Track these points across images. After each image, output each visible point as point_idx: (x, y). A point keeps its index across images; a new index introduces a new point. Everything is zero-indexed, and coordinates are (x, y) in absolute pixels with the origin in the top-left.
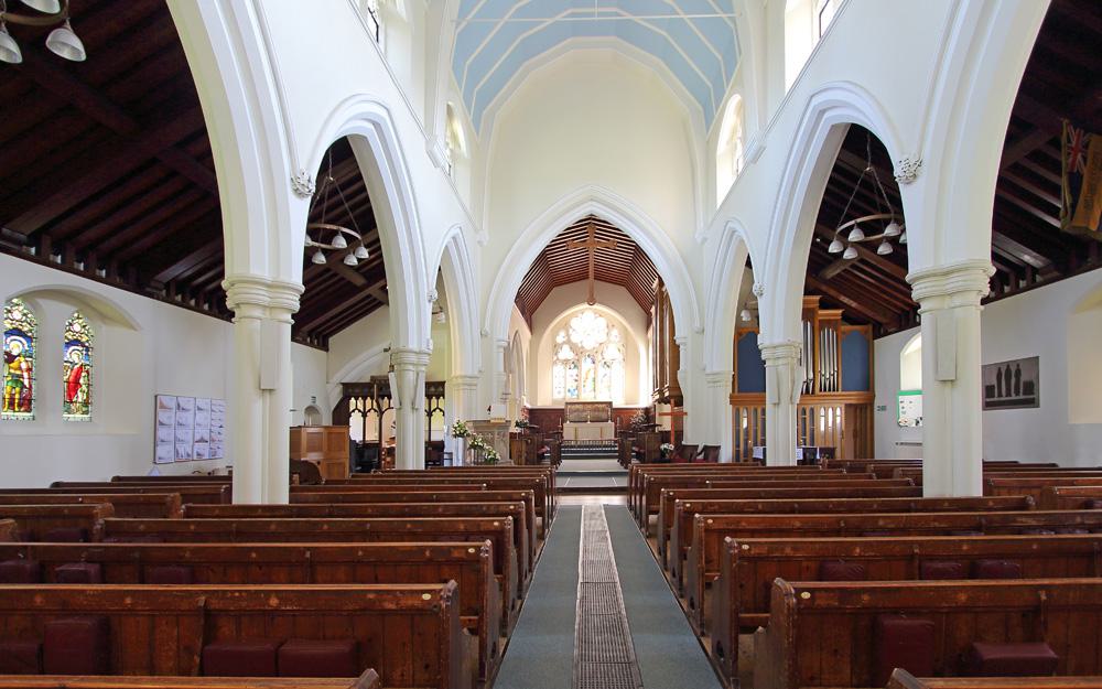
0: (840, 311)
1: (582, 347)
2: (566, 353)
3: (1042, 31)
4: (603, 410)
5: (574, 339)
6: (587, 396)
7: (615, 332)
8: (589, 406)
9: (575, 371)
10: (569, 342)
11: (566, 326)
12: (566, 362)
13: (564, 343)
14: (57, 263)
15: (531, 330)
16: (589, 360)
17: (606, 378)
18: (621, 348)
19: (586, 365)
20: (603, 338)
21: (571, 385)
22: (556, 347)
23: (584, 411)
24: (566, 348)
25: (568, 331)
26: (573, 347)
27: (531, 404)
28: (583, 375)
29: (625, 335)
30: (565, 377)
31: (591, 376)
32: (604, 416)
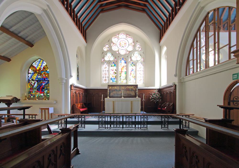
0: (2, 126)
1: (119, 53)
2: (109, 57)
3: (73, 121)
4: (132, 90)
5: (114, 48)
6: (122, 81)
7: (138, 46)
8: (123, 88)
9: (115, 68)
10: (110, 50)
11: (109, 41)
12: (109, 62)
13: (108, 51)
14: (228, 109)
15: (85, 39)
16: (123, 61)
17: (133, 72)
18: (142, 54)
19: (122, 64)
20: (130, 49)
21: (112, 75)
22: (104, 54)
23: (120, 90)
24: (109, 55)
25: (110, 45)
26: (114, 54)
27: (221, 60)
28: (120, 70)
29: (145, 47)
30: (108, 71)
31: (124, 70)
32: (133, 94)
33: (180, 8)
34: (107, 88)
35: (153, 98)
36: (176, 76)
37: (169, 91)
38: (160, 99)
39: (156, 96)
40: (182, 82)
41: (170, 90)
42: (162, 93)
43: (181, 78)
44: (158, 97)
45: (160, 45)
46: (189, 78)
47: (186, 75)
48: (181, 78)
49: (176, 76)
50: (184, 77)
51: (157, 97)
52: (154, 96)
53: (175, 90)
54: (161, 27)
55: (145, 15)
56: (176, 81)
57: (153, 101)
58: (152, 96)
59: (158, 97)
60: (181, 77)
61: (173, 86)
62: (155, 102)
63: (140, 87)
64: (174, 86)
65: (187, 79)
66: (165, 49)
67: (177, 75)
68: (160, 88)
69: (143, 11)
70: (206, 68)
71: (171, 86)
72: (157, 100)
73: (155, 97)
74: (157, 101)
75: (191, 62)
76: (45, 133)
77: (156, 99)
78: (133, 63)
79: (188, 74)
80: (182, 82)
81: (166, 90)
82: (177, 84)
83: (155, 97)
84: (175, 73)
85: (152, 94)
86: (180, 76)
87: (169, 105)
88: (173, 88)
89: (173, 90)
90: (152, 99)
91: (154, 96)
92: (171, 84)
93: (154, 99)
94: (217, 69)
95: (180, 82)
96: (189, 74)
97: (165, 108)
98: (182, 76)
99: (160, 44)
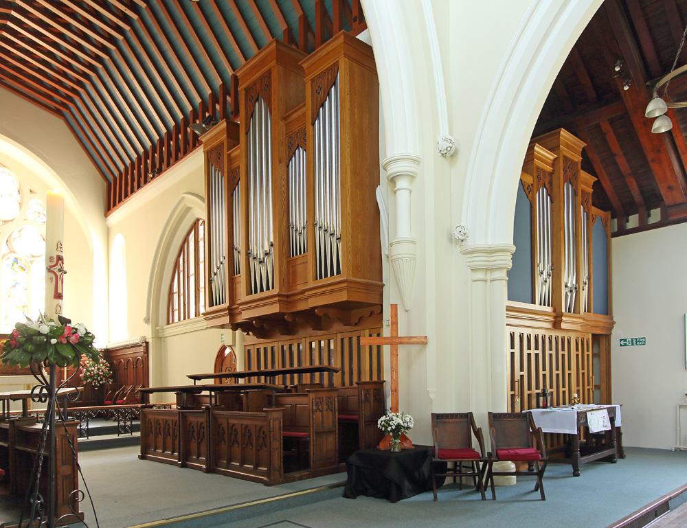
33: (154, 177)
34: (606, 410)
35: (89, 375)
36: (147, 321)
37: (132, 355)
38: (110, 377)
39: (98, 369)
40: (161, 338)
41: (136, 355)
42: (115, 362)
43: (157, 328)
44: (102, 371)
45: (108, 222)
46: (179, 329)
47: (168, 323)
48: (157, 328)
49: (147, 321)
50: (165, 327)
51: (101, 373)
52: (93, 368)
53: (146, 355)
54: (111, 178)
55: (59, 122)
56: (146, 332)
57: (91, 383)
58: (88, 371)
59: (102, 371)
60: (158, 326)
61: (141, 346)
62: (96, 386)
63: (496, 470)
64: (144, 344)
65: (169, 330)
66: (118, 240)
67: (149, 319)
68: (109, 347)
69: (58, 112)
70: (196, 316)
71: (134, 346)
72: (101, 379)
73: (96, 371)
74: (101, 382)
75: (176, 296)
76: (108, 367)
77: (97, 379)
78: (16, 260)
79: (171, 322)
80: (159, 337)
81: (120, 353)
82: (150, 341)
83: (96, 371)
84: (145, 315)
85: (85, 365)
86: (156, 324)
87: (133, 390)
88: (141, 349)
89: (142, 354)
90: (86, 377)
91: (93, 368)
92: (136, 339)
93: (94, 379)
94: (192, 327)
95: (155, 337)
96: (173, 321)
97: (125, 399)
98: (160, 324)
99: (106, 221)
